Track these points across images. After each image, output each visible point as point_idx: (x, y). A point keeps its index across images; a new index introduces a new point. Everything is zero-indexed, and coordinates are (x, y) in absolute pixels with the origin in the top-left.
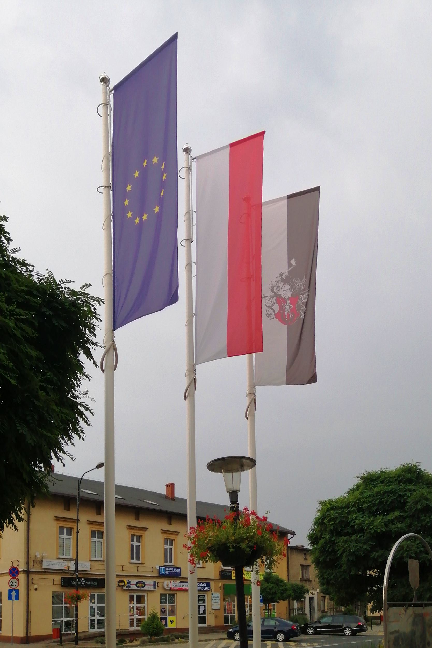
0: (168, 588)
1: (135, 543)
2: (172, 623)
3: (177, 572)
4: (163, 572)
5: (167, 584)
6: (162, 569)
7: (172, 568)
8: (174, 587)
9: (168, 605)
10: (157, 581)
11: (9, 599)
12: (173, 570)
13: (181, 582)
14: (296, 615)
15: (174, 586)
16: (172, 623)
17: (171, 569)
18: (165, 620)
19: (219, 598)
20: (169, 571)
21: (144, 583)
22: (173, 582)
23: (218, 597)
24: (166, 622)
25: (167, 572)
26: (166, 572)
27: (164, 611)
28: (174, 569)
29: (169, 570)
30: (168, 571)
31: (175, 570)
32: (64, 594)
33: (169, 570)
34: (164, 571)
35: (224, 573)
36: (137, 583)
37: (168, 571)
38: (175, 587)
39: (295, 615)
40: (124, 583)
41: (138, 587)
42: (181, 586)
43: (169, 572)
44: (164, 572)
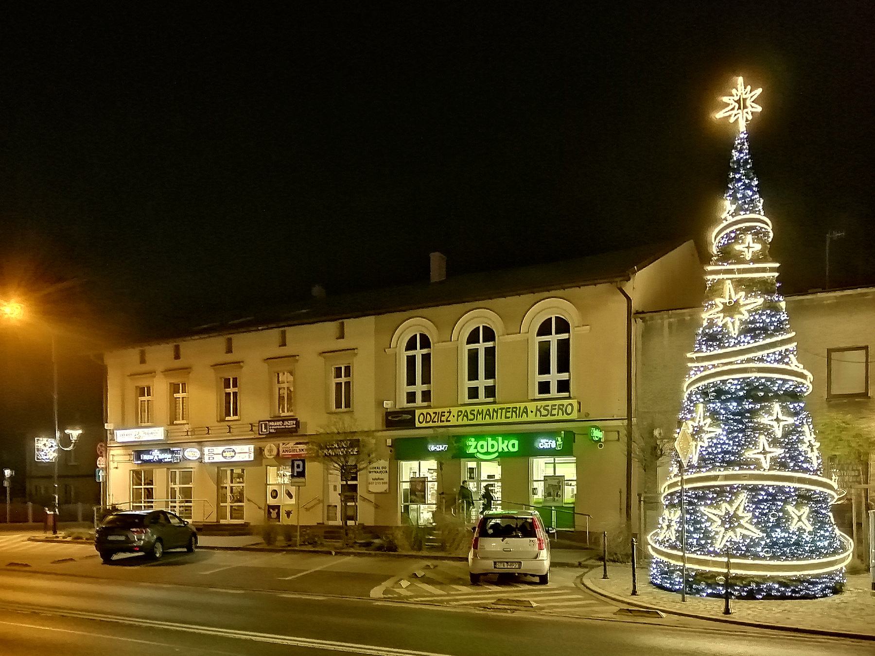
0: (271, 455)
1: (231, 390)
2: (288, 516)
3: (289, 427)
4: (265, 431)
5: (269, 449)
6: (263, 425)
7: (279, 421)
8: (284, 453)
9: (143, 487)
10: (261, 444)
11: (488, 476)
12: (283, 425)
13: (297, 444)
14: (777, 265)
15: (283, 451)
16: (288, 516)
17: (278, 423)
18: (276, 511)
19: (387, 470)
20: (275, 427)
21: (234, 451)
22: (283, 444)
23: (385, 468)
24: (278, 514)
25: (272, 429)
26: (269, 429)
27: (275, 495)
28: (284, 423)
29: (275, 426)
30: (273, 427)
31: (286, 423)
32: (143, 472)
33: (275, 426)
34: (266, 428)
35: (392, 417)
36: (224, 451)
37: (273, 427)
38: (287, 453)
39: (772, 270)
40: (224, 455)
41: (225, 457)
42: (298, 451)
43: (274, 429)
44: (267, 430)
